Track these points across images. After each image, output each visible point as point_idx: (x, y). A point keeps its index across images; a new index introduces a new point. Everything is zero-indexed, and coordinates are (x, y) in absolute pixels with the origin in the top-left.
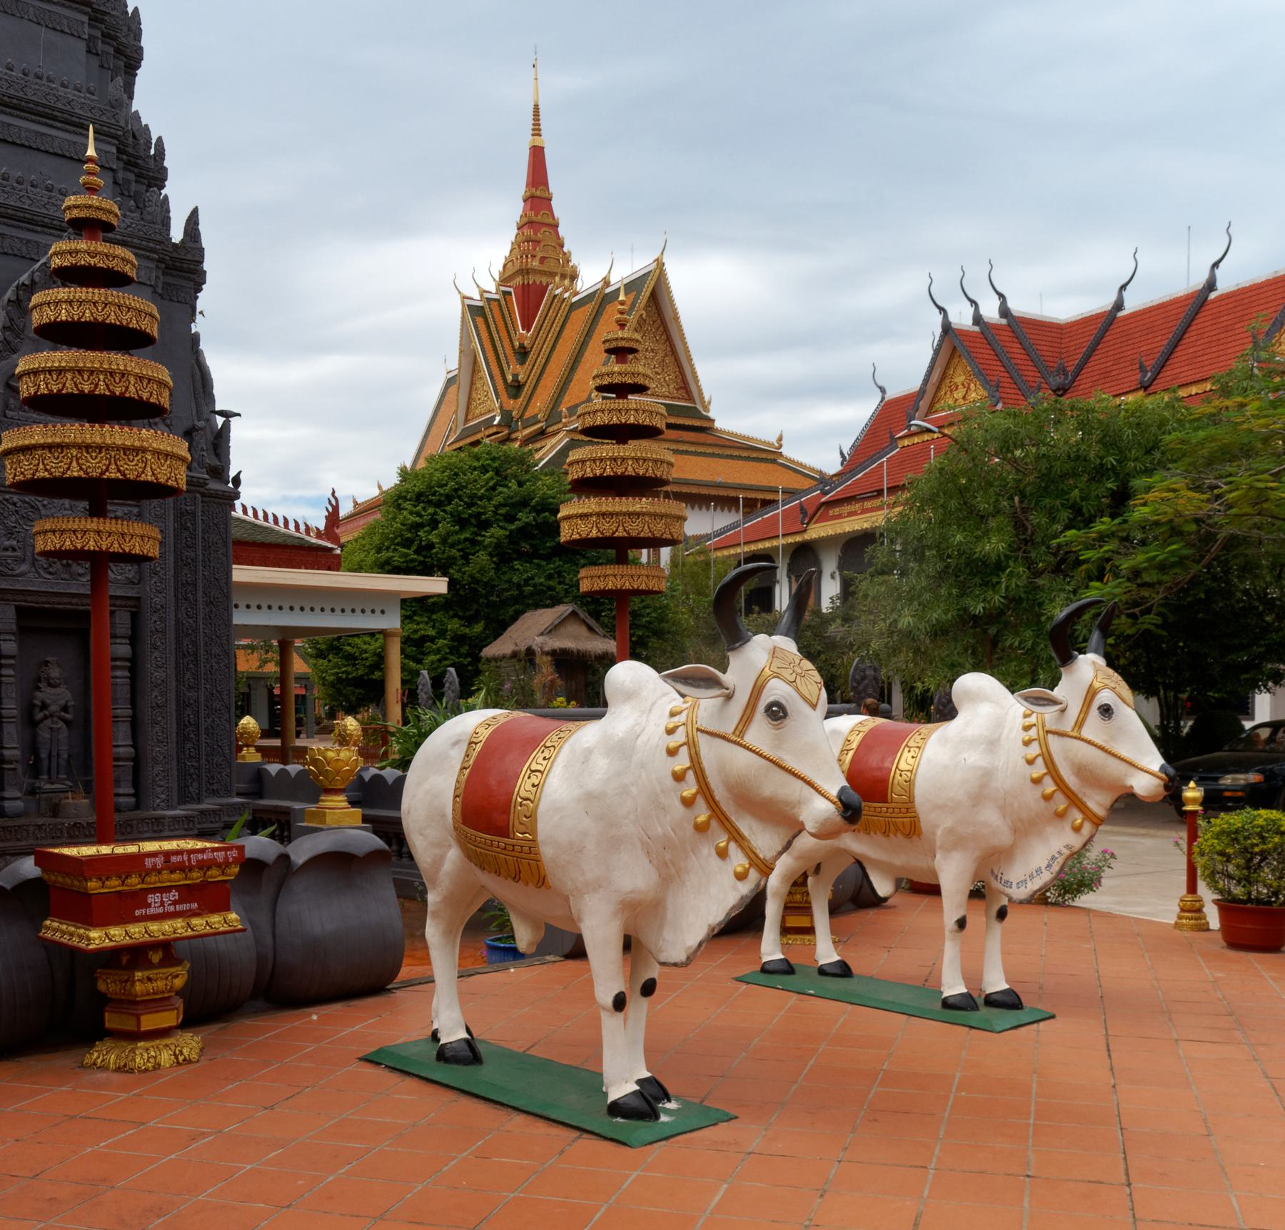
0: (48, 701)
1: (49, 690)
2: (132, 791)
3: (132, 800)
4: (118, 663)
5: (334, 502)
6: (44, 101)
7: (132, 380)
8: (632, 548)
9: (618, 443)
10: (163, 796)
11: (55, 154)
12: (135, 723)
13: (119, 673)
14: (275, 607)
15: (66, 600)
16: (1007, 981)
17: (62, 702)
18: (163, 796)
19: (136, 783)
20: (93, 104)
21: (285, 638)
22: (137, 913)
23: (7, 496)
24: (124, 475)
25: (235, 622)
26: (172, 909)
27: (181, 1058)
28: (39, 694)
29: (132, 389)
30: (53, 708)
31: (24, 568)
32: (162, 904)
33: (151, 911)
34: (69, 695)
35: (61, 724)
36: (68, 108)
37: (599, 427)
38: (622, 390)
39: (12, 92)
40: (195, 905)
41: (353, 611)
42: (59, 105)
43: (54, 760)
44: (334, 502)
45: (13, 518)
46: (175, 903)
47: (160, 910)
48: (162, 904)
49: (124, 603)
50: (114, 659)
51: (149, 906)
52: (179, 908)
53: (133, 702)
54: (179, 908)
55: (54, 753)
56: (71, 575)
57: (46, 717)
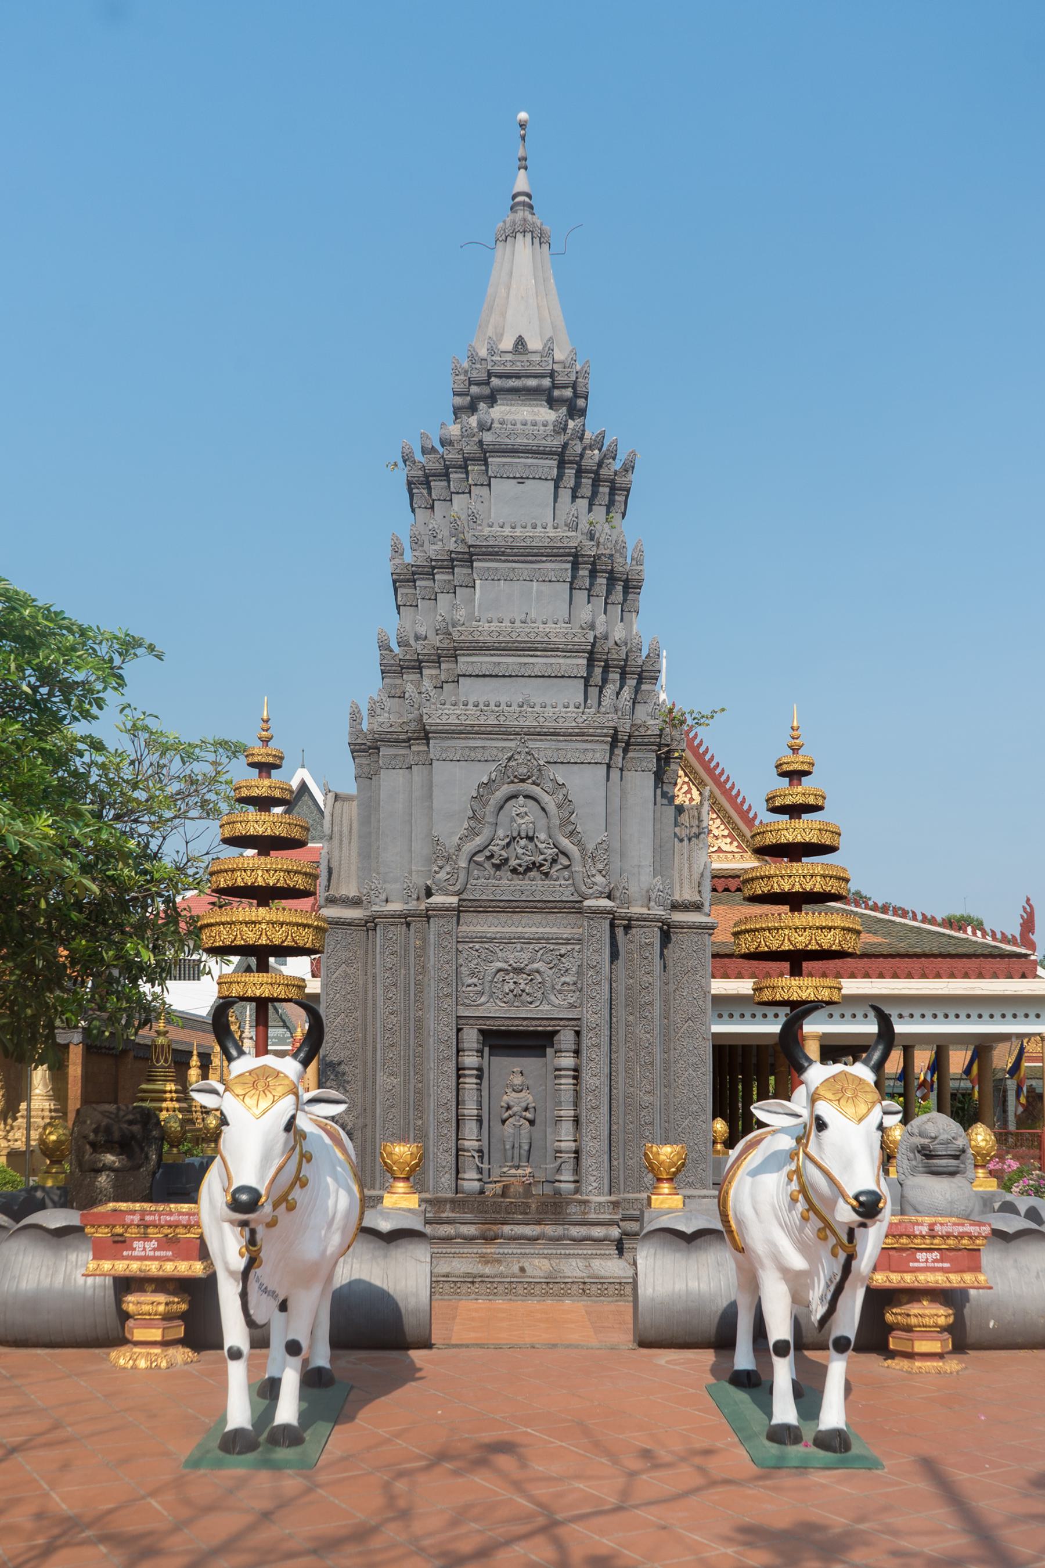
0: (512, 1104)
1: (514, 1095)
2: (572, 1179)
3: (572, 1186)
4: (562, 1073)
5: (1028, 910)
6: (527, 639)
7: (260, 873)
8: (805, 960)
9: (791, 861)
10: (595, 1184)
11: (536, 676)
12: (577, 1121)
13: (563, 1081)
14: (917, 1015)
15: (517, 1022)
16: (847, 1425)
17: (524, 1105)
18: (595, 1184)
19: (576, 1171)
20: (566, 631)
21: (941, 1047)
22: (125, 1253)
23: (471, 945)
24: (271, 941)
25: (896, 1031)
26: (151, 1254)
27: (154, 1364)
28: (505, 1097)
29: (260, 879)
30: (515, 1109)
31: (483, 999)
32: (144, 1249)
33: (135, 1253)
34: (530, 1098)
35: (523, 1121)
36: (546, 639)
37: (782, 845)
38: (795, 811)
39: (501, 638)
40: (170, 1253)
41: (957, 1016)
42: (538, 639)
43: (516, 1151)
44: (1028, 910)
45: (475, 962)
46: (154, 1250)
47: (143, 1254)
48: (144, 1249)
49: (567, 1023)
50: (557, 1070)
51: (134, 1249)
52: (158, 1253)
53: (576, 1105)
54: (158, 1253)
55: (517, 1145)
56: (522, 1003)
57: (511, 1116)
